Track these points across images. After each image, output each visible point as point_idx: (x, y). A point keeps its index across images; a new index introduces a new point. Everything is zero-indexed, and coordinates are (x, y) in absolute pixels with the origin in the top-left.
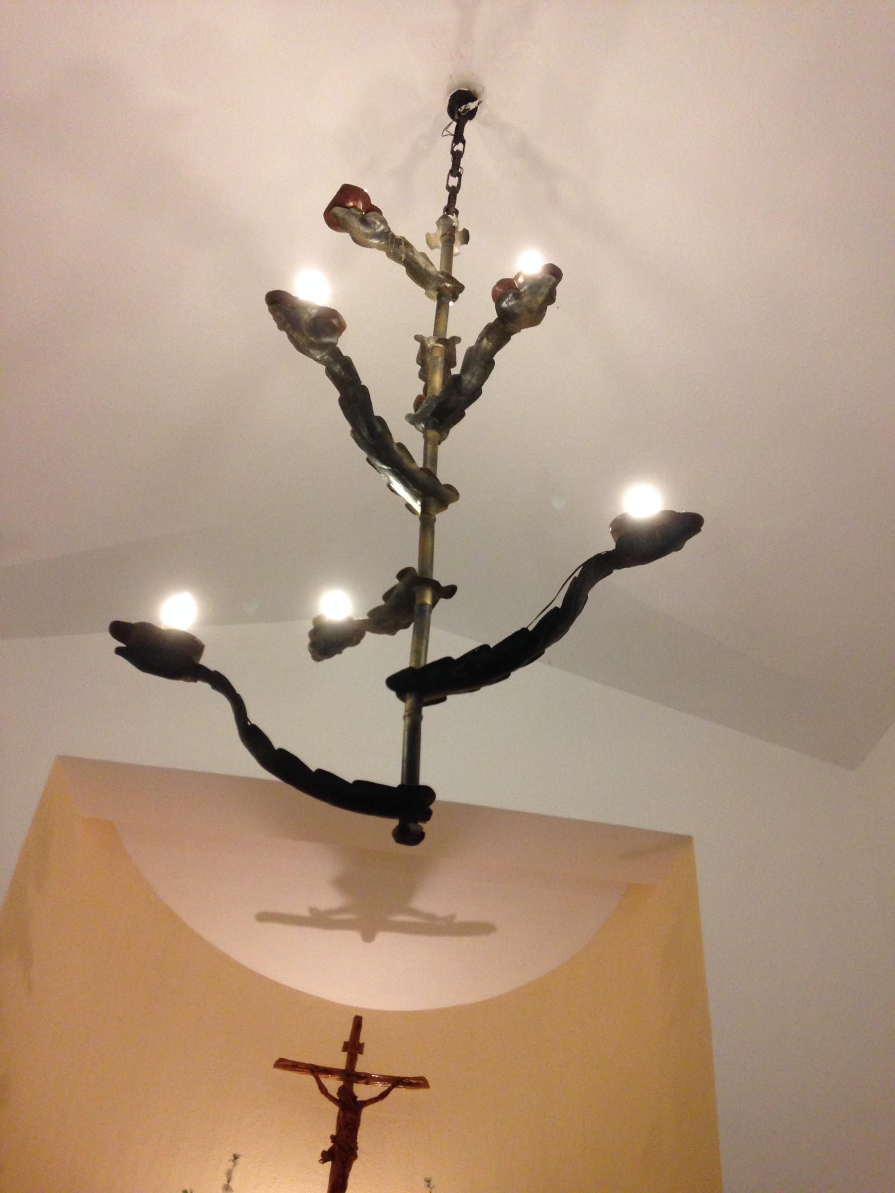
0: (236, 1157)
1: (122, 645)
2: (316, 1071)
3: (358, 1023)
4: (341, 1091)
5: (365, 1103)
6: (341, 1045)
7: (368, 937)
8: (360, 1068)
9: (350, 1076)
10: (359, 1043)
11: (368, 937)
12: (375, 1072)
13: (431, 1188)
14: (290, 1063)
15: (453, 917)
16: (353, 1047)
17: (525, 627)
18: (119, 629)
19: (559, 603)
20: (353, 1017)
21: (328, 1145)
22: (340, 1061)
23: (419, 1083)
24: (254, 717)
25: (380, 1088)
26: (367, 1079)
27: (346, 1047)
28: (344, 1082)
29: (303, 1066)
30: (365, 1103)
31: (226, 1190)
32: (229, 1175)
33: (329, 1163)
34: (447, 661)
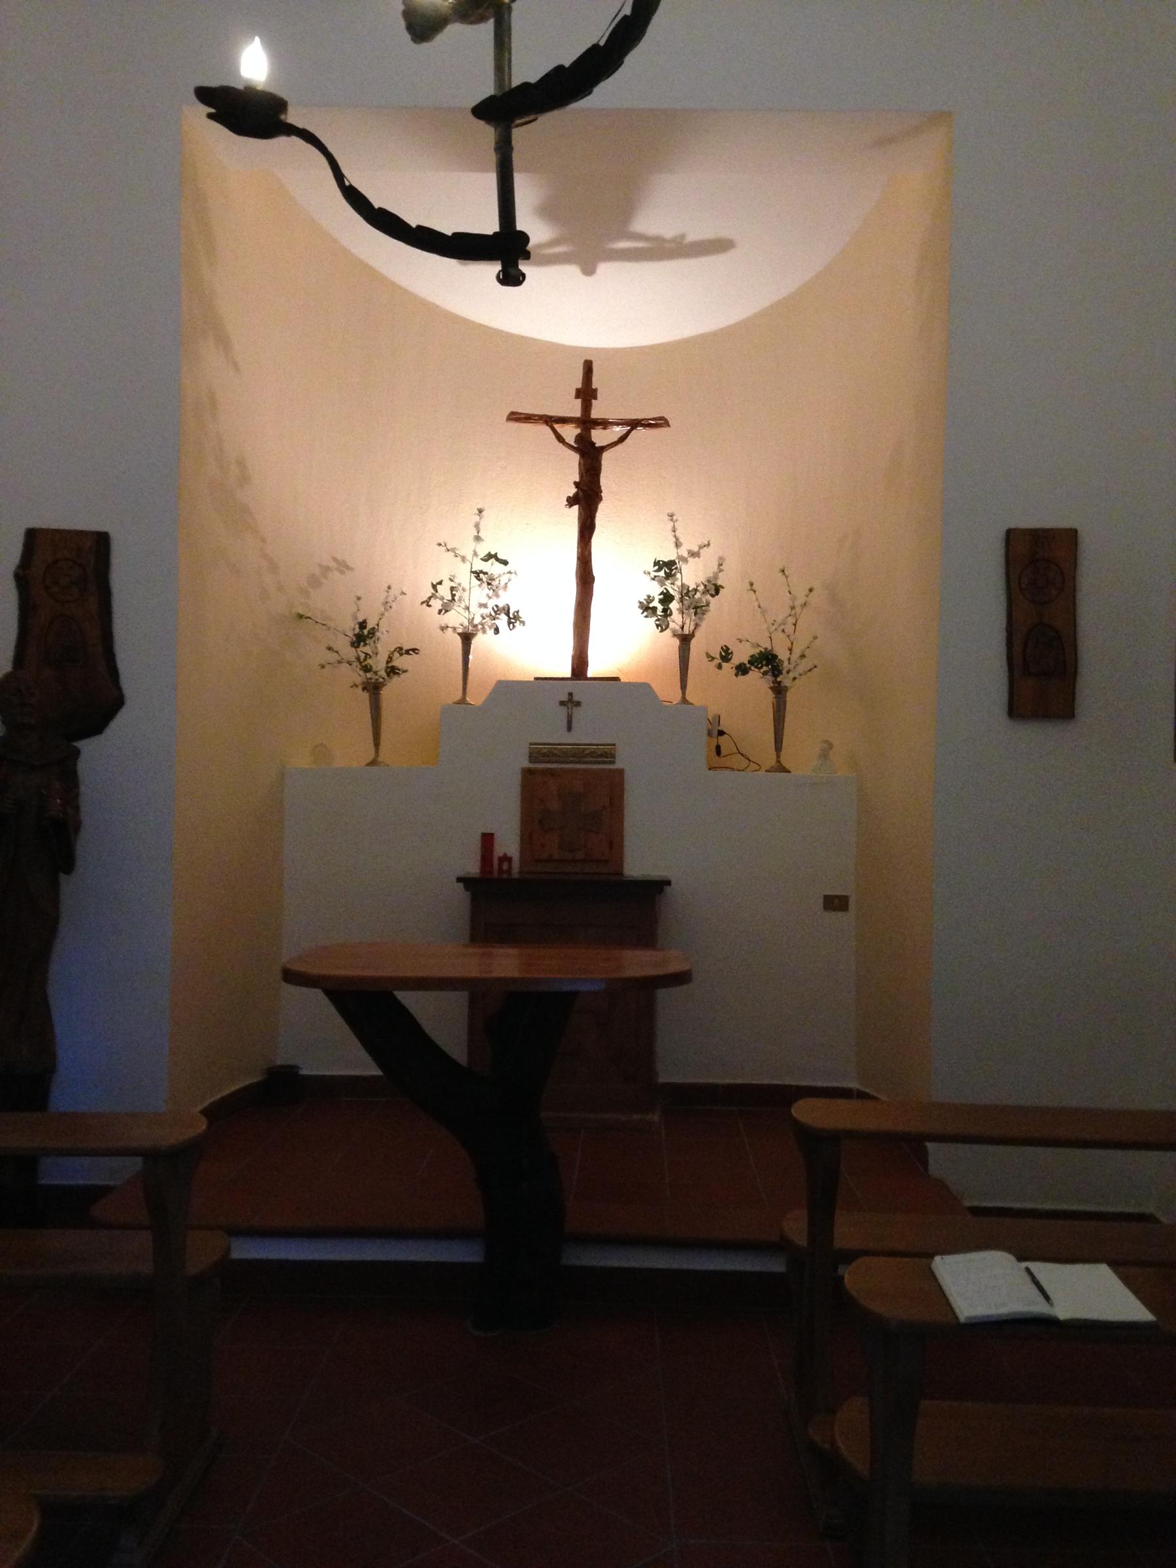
0: (480, 511)
1: (213, 111)
2: (550, 421)
3: (588, 368)
4: (579, 439)
5: (603, 449)
6: (574, 393)
7: (589, 270)
8: (595, 414)
9: (587, 423)
10: (593, 389)
11: (589, 270)
12: (611, 416)
13: (674, 522)
14: (522, 416)
15: (683, 236)
16: (587, 394)
17: (595, 42)
18: (205, 95)
19: (627, 11)
20: (583, 361)
21: (572, 491)
22: (574, 409)
23: (660, 423)
24: (353, 178)
25: (619, 430)
26: (605, 424)
27: (579, 394)
28: (581, 430)
29: (536, 418)
30: (603, 449)
31: (477, 540)
32: (477, 526)
33: (576, 508)
34: (525, 86)
